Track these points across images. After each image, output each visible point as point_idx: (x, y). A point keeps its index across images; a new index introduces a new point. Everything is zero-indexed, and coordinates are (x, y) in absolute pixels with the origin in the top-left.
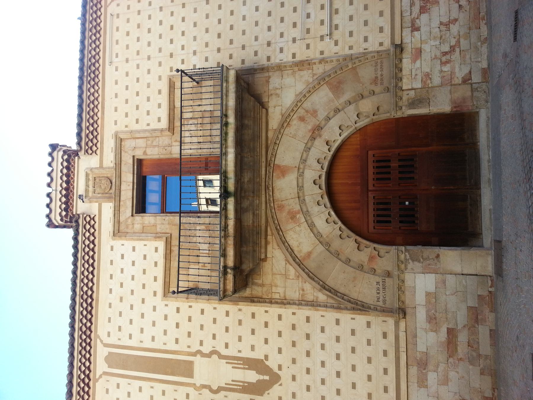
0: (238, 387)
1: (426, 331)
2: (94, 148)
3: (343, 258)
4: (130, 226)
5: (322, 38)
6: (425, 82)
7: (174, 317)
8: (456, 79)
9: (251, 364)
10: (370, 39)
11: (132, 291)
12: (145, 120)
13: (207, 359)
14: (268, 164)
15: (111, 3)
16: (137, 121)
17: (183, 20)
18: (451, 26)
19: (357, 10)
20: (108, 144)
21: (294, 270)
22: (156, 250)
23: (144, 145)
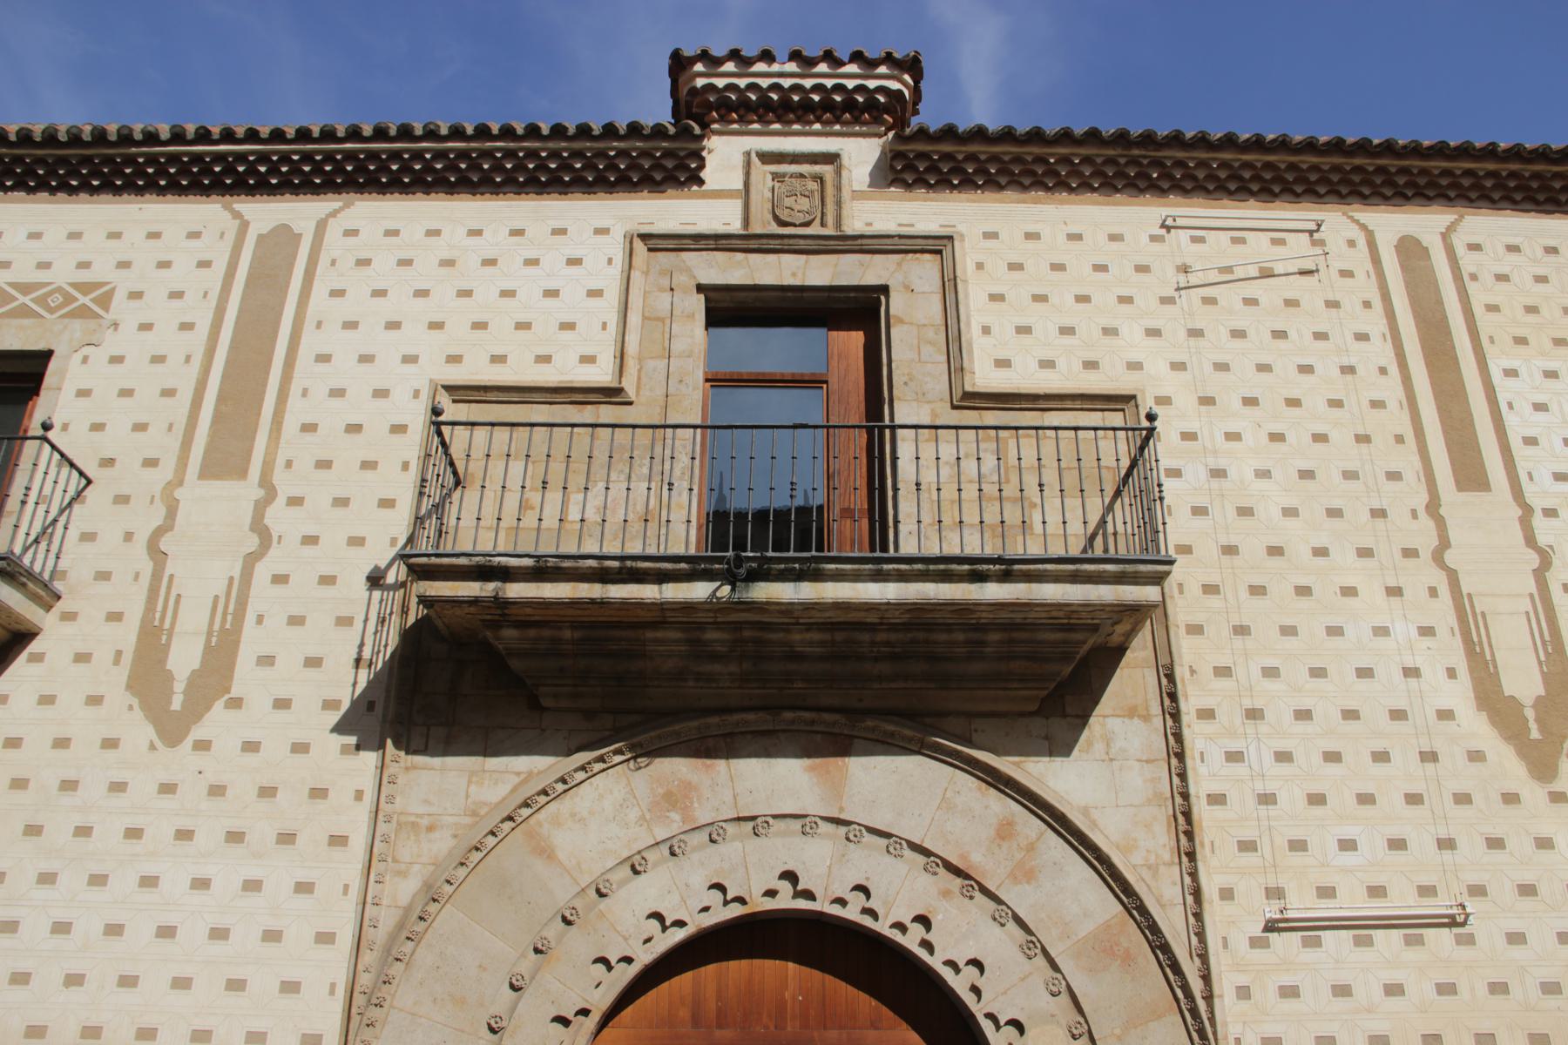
0: (158, 615)
5: (1275, 893)
9: (221, 653)
13: (248, 520)
15: (1357, 222)
17: (1320, 438)
19: (1369, 1011)
22: (588, 359)
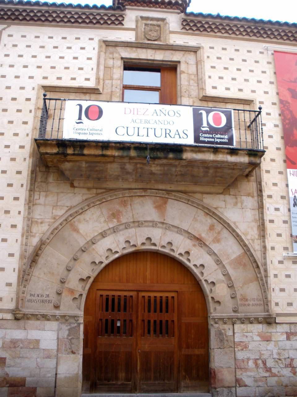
1: (3, 338)
2: (188, 28)
3: (108, 232)
4: (111, 56)
6: (239, 345)
7: (21, 96)
8: (241, 372)
10: (282, 294)
11: (49, 57)
12: (215, 75)
14: (168, 192)
16: (213, 67)
18: (290, 369)
20: (191, 40)
21: (61, 214)
22: (88, 79)
23: (190, 72)
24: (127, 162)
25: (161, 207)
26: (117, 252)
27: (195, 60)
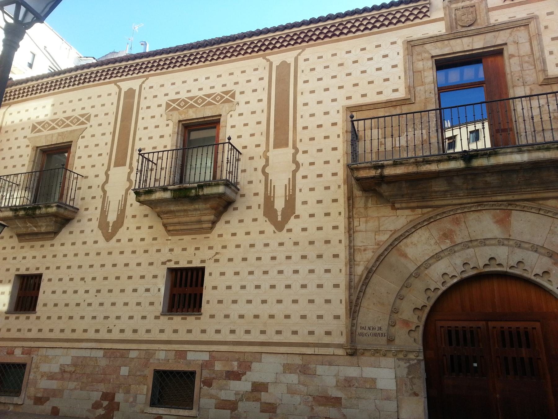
11: (350, 74)
14: (510, 202)
21: (385, 239)
22: (395, 90)
23: (522, 53)
24: (433, 249)
25: (503, 222)
26: (500, 265)
27: (528, 36)
